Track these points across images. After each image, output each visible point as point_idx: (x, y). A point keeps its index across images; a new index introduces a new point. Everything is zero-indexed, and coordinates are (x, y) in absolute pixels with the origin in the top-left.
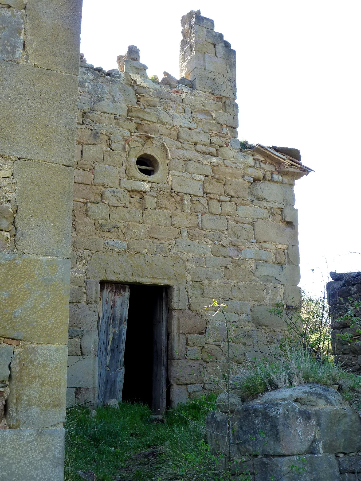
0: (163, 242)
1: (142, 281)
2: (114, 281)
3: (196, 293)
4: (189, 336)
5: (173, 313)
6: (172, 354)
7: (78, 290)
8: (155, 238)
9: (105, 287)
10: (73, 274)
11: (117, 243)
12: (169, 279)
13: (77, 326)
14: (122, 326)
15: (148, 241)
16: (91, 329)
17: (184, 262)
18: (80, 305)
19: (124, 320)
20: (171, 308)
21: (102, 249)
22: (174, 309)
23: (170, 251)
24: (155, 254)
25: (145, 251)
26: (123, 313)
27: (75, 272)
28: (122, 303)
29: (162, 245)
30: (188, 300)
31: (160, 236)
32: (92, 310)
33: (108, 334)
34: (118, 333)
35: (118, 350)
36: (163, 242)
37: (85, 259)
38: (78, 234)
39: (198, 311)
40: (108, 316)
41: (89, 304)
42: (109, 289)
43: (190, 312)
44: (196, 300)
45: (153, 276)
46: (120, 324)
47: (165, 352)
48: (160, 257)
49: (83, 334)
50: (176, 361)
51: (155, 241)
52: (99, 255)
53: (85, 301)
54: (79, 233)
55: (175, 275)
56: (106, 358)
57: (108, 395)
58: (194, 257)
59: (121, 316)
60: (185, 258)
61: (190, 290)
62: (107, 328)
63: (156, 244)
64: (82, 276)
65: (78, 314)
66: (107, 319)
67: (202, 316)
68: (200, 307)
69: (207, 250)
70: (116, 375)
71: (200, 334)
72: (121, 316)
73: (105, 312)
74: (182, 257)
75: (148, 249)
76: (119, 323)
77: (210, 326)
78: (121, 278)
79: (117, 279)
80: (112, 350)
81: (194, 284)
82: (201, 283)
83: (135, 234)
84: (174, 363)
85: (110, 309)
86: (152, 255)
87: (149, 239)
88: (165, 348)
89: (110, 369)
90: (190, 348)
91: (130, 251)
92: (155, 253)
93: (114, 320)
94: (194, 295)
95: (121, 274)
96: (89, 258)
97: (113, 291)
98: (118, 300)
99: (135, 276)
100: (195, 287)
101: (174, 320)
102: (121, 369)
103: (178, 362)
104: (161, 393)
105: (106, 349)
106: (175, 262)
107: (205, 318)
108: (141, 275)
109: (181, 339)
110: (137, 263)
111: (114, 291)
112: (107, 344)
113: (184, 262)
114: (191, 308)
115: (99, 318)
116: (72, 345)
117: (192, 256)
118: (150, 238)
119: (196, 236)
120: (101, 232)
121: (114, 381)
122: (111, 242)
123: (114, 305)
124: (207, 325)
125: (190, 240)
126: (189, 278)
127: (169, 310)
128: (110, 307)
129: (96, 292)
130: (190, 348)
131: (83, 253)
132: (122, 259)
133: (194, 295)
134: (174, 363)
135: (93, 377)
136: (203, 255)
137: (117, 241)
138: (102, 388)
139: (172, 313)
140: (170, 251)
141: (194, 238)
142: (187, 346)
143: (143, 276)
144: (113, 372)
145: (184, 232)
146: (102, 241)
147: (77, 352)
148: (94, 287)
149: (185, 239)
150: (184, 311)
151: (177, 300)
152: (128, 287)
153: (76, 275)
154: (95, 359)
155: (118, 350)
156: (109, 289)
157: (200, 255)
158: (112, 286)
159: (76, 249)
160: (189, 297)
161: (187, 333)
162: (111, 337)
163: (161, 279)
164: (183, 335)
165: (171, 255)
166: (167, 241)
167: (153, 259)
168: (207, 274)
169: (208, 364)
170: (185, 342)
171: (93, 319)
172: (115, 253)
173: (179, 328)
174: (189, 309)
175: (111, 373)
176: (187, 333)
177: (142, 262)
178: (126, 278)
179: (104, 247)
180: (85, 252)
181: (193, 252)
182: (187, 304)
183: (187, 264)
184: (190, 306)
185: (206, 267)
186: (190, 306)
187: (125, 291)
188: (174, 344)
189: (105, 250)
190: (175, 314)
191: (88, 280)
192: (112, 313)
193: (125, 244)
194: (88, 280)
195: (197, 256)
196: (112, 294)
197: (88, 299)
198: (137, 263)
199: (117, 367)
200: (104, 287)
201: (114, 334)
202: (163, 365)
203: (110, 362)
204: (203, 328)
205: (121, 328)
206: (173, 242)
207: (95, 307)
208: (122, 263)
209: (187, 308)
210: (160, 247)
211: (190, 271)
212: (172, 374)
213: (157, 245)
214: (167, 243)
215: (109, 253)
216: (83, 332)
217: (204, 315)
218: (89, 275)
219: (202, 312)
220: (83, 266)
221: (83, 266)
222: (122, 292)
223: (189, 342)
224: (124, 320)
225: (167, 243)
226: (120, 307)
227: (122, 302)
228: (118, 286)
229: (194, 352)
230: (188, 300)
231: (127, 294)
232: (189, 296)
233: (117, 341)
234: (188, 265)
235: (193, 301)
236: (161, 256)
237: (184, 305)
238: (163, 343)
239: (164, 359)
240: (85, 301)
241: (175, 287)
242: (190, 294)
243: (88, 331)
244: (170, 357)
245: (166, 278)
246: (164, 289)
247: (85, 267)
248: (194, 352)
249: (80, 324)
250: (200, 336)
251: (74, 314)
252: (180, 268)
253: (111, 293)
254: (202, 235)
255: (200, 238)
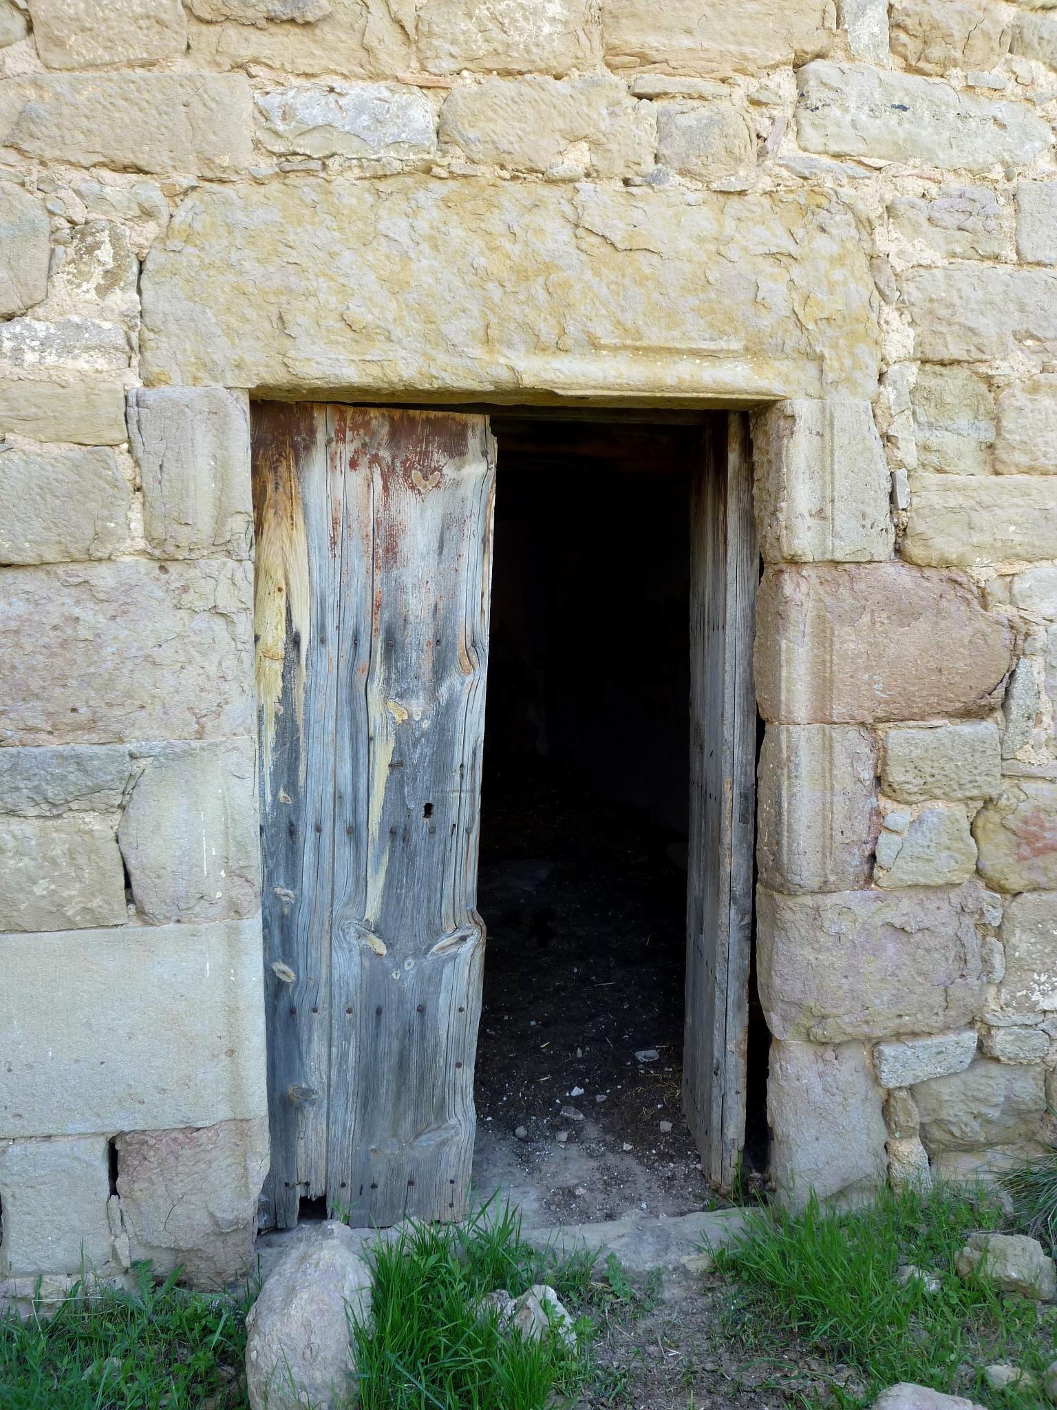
0: (709, 87)
1: (562, 378)
2: (352, 389)
3: (949, 441)
4: (897, 737)
5: (788, 589)
6: (777, 856)
7: (76, 467)
8: (646, 60)
9: (321, 437)
10: (30, 357)
11: (360, 109)
12: (755, 351)
13: (91, 725)
14: (453, 680)
15: (595, 84)
16: (200, 735)
17: (866, 225)
18: (104, 577)
19: (462, 641)
20: (771, 554)
21: (248, 159)
22: (795, 562)
23: (762, 154)
24: (652, 181)
25: (577, 158)
26: (453, 595)
27: (45, 344)
28: (441, 537)
29: (704, 111)
30: (892, 497)
31: (687, 42)
32: (199, 605)
33: (361, 741)
34: (426, 725)
35: (432, 831)
36: (709, 87)
37: (116, 240)
38: (55, 58)
39: (962, 565)
40: (350, 624)
41: (172, 567)
42: (347, 450)
43: (902, 576)
44: (945, 488)
45: (638, 335)
46: (440, 671)
47: (744, 820)
48: (691, 197)
49: (131, 783)
50: (809, 900)
51: (650, 81)
52: (227, 202)
53: (141, 544)
54: (59, 43)
55: (801, 325)
56: (360, 883)
57: (386, 1090)
58: (934, 190)
59: (442, 616)
60: (870, 196)
61: (901, 427)
62: (352, 700)
63: (656, 105)
64: (102, 363)
65: (95, 643)
66: (347, 644)
67: (983, 596)
68: (976, 538)
69: (1026, 135)
70: (431, 980)
71: (968, 714)
72: (442, 616)
73: (331, 600)
74: (847, 191)
75: (595, 145)
76: (427, 666)
77: (1038, 663)
78: (407, 365)
79: (375, 371)
80: (397, 834)
81: (931, 383)
82: (983, 369)
83: (496, 33)
84: (793, 912)
85: (359, 579)
86: (626, 182)
87: (602, 70)
88: (744, 796)
89: (389, 946)
90: (898, 815)
91: (459, 165)
92: (649, 166)
93: (392, 646)
94: (934, 459)
95: (397, 332)
96: (151, 229)
97: (375, 459)
98: (418, 517)
99: (510, 345)
100: (941, 404)
101: (791, 634)
102: (463, 939)
103: (817, 909)
104: (717, 1054)
105: (353, 832)
106: (800, 233)
107: (1006, 611)
108: (547, 330)
109: (841, 760)
110: (515, 250)
111: (385, 454)
112: (359, 801)
113: (866, 225)
114: (914, 549)
115: (295, 641)
116: (53, 862)
117: (918, 186)
118: (614, 58)
119: (947, 37)
120: (232, 32)
121: (421, 1010)
122: (310, 104)
123: (391, 550)
124: (1016, 653)
125: (909, 69)
126: (900, 339)
127: (766, 566)
128: (359, 564)
129: (222, 475)
130: (898, 815)
131: (101, 199)
132: (403, 224)
133: (934, 459)
134: (788, 915)
135: (231, 1053)
136: (998, 173)
137: (357, 90)
138: (344, 1056)
139: (778, 587)
140: (762, 154)
141: (936, 52)
142: (884, 803)
143: (568, 342)
144: (410, 964)
145: (861, 11)
146: (241, 96)
147: (96, 903)
148: (204, 440)
149: (869, 60)
150: (863, 570)
151: (818, 495)
152: (479, 422)
153: (51, 359)
154: (233, 935)
155: (432, 831)
156: (347, 450)
157: (979, 175)
158: (366, 425)
159: (37, 172)
160: (901, 474)
161: (879, 720)
162: (383, 755)
163: (694, 353)
164: (853, 733)
165: (767, 183)
166: (739, 78)
167: (637, 215)
168: (1022, 308)
169: (1014, 907)
170: (867, 775)
171: (212, 669)
172: (347, 187)
173: (824, 687)
174: (898, 551)
175: (399, 965)
176: (879, 720)
177: (555, 236)
178: (442, 358)
179: (257, 144)
180: (116, 185)
181: (930, 156)
182: (884, 521)
183: (888, 240)
184: (902, 531)
185: (1021, 262)
186: (902, 531)
187: (456, 448)
188: (792, 796)
189: (266, 166)
190: (799, 597)
191: (151, 396)
192: (377, 606)
193: (422, 113)
194: (151, 396)
195: (954, 184)
196: (369, 482)
197: (159, 532)
198: (515, 250)
199: (435, 933)
200: (312, 432)
201: (404, 735)
202: (725, 898)
203: (385, 906)
204: (994, 679)
205: (444, 691)
206: (784, 82)
207: (224, 584)
208: (405, 257)
209: (883, 549)
210: (683, 121)
211: (909, 287)
212: (777, 981)
213: (663, 113)
214: (739, 93)
215: (306, 188)
216: (136, 767)
217: (997, 589)
218: (161, 355)
219: (984, 572)
220: (102, 291)
221: (102, 291)
222: (439, 458)
223: (896, 775)
224: (462, 641)
225: (739, 93)
226: (433, 557)
227: (444, 529)
228: (412, 418)
229: (923, 839)
230: (892, 497)
231: (473, 475)
232: (901, 464)
233: (424, 778)
234: (892, 248)
235: (926, 497)
236: (693, 192)
237: (860, 533)
238: (726, 768)
239: (733, 866)
240: (141, 544)
241: (803, 408)
242: (908, 452)
243: (171, 758)
244: (764, 875)
245: (736, 345)
246: (734, 428)
247: (122, 299)
248: (923, 839)
249: (118, 712)
250: (967, 729)
251: (64, 644)
252: (838, 275)
253: (363, 471)
254: (995, 33)
255: (976, 56)
